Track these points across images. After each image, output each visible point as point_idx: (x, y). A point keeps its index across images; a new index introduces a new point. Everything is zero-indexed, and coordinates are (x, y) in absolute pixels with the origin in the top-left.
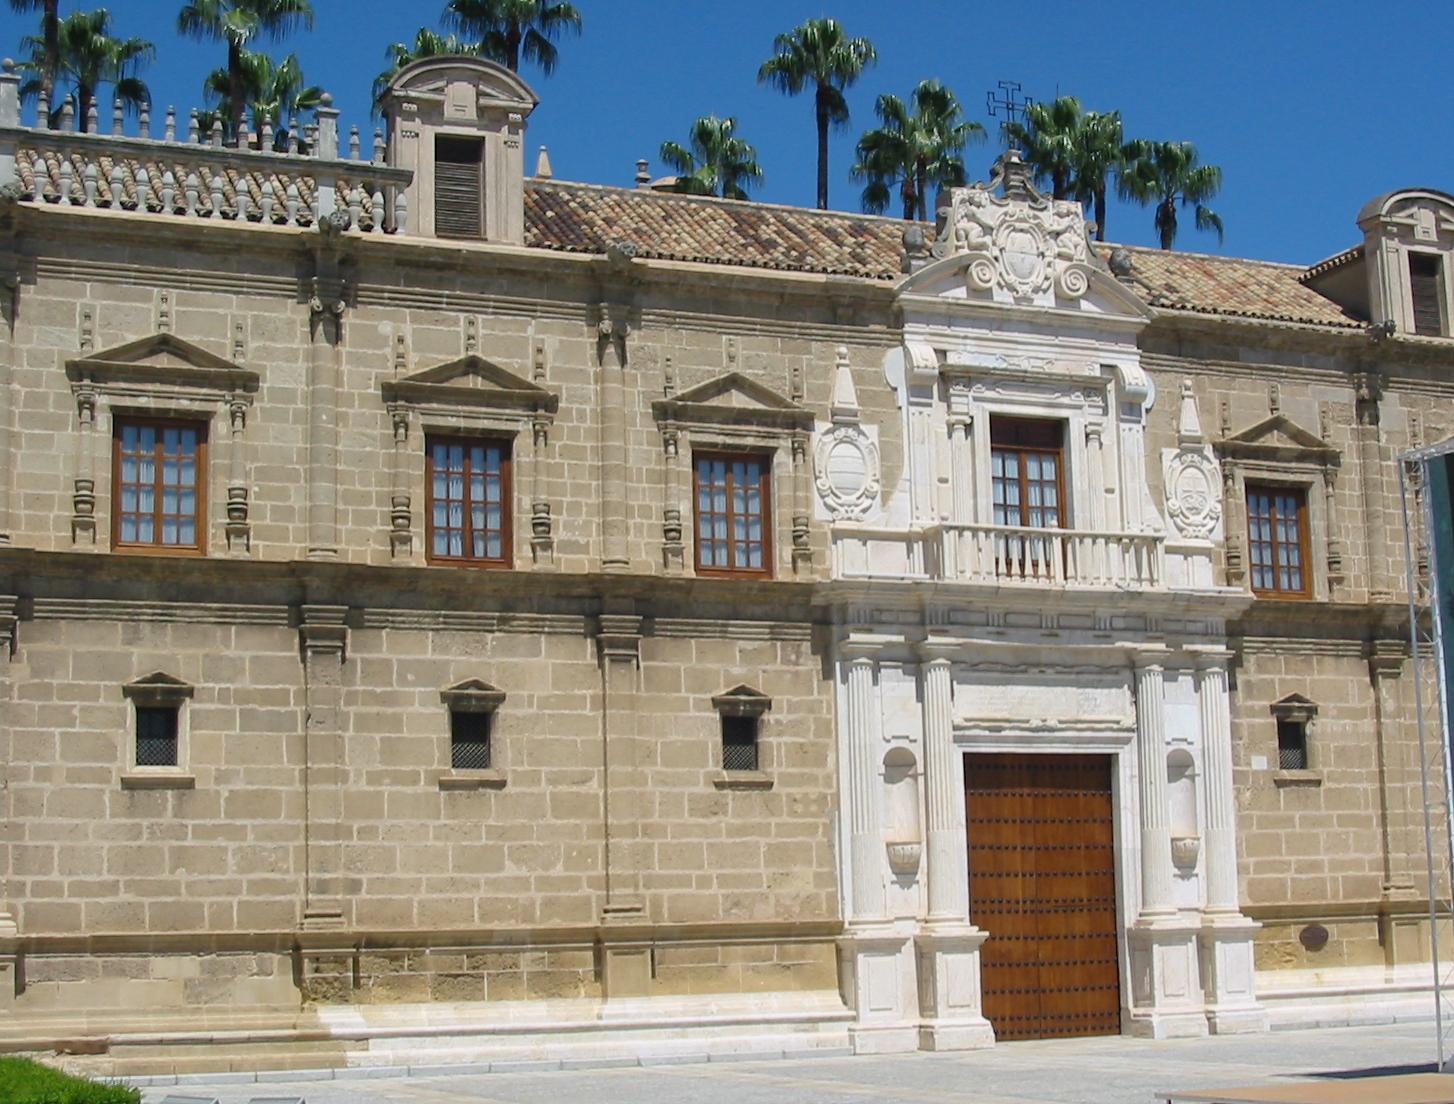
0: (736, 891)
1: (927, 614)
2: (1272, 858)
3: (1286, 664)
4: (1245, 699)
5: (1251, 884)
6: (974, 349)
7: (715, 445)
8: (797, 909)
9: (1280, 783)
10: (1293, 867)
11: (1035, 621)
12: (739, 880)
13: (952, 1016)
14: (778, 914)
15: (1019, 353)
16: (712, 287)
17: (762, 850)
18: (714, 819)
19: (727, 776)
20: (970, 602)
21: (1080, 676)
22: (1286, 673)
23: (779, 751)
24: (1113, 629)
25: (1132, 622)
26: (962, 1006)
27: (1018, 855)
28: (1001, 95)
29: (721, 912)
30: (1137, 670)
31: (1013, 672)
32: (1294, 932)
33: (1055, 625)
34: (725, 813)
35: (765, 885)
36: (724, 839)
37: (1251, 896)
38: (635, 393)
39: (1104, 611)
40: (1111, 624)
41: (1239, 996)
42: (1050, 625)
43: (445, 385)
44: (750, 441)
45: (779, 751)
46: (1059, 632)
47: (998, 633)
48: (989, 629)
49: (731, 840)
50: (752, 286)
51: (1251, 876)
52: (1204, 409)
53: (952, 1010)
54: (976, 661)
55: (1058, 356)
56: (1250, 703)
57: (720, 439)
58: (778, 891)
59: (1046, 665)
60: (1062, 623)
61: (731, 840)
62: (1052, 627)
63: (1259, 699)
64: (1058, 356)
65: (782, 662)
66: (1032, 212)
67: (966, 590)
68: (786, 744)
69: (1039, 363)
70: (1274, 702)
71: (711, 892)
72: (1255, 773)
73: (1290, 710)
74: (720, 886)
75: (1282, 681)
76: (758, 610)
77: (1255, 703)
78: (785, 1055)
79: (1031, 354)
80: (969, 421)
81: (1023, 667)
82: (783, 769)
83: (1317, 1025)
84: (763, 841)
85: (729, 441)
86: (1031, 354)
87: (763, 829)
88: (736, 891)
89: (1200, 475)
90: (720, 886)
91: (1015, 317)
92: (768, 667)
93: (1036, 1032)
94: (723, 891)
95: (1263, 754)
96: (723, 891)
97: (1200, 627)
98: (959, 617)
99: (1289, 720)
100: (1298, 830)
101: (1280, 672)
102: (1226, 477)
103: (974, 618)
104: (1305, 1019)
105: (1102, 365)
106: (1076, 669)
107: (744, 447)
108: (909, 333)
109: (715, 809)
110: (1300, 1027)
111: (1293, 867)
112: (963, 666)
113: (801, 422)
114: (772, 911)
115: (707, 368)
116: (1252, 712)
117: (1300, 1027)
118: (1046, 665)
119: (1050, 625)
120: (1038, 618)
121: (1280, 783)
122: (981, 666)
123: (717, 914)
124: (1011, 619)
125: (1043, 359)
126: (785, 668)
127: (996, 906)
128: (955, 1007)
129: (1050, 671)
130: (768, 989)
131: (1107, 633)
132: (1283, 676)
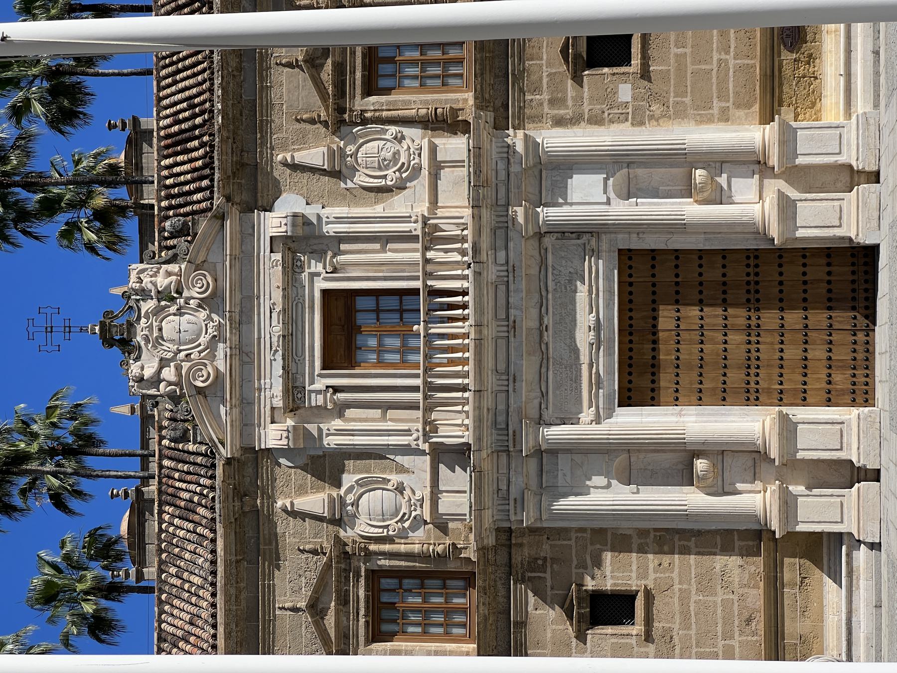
0: (736, 623)
1: (499, 449)
2: (714, 80)
3: (532, 59)
4: (567, 108)
5: (738, 106)
6: (268, 381)
7: (367, 622)
8: (753, 568)
9: (645, 74)
10: (723, 56)
11: (502, 343)
12: (727, 620)
13: (849, 445)
14: (756, 587)
15: (268, 336)
16: (236, 626)
17: (701, 598)
18: (676, 639)
19: (637, 628)
20: (488, 409)
21: (550, 289)
22: (542, 59)
23: (618, 578)
24: (507, 262)
25: (500, 243)
26: (842, 436)
27: (707, 347)
28: (40, 321)
29: (755, 638)
30: (543, 230)
31: (548, 359)
32: (787, 57)
33: (505, 268)
34: (671, 630)
35: (731, 596)
36: (693, 632)
37: (749, 106)
39: (492, 273)
40: (502, 265)
41: (844, 141)
42: (505, 329)
43: (333, 635)
44: (362, 593)
45: (618, 578)
46: (512, 318)
47: (514, 382)
48: (511, 390)
49: (694, 626)
50: (233, 591)
51: (730, 104)
52: (303, 141)
53: (845, 445)
54: (539, 394)
55: (267, 296)
56: (570, 103)
57: (362, 621)
58: (736, 585)
59: (541, 325)
60: (504, 262)
61: (694, 626)
62: (508, 326)
63: (565, 91)
64: (267, 296)
65: (545, 572)
66: (143, 320)
67: (479, 421)
68: (612, 572)
69: (275, 315)
70: (570, 77)
71: (737, 645)
72: (634, 98)
73: (577, 56)
74: (732, 637)
75: (549, 65)
76: (502, 592)
77: (569, 95)
78: (878, 606)
80: (331, 390)
81: (543, 347)
82: (634, 575)
83: (876, 53)
84: (694, 598)
85: (362, 612)
87: (684, 597)
88: (736, 623)
89: (366, 496)
90: (732, 637)
91: (235, 339)
92: (549, 584)
93: (868, 335)
94: (737, 634)
95: (618, 86)
96: (737, 634)
97: (501, 166)
98: (501, 418)
99: (585, 56)
100: (688, 50)
101: (541, 66)
102: (364, 122)
103: (502, 407)
104: (870, 63)
105: (272, 251)
106: (544, 293)
107: (367, 597)
108: (260, 445)
109: (668, 638)
110: (877, 74)
111: (723, 56)
112: (543, 406)
114: (754, 592)
115: (303, 629)
116: (578, 100)
117: (877, 74)
118: (541, 325)
119: (505, 329)
120: (499, 341)
121: (645, 74)
122: (544, 390)
123: (757, 641)
124: (502, 367)
125: (271, 312)
126: (549, 570)
127: (752, 287)
128: (842, 443)
129: (546, 320)
130: (821, 606)
131: (511, 269)
132: (544, 62)
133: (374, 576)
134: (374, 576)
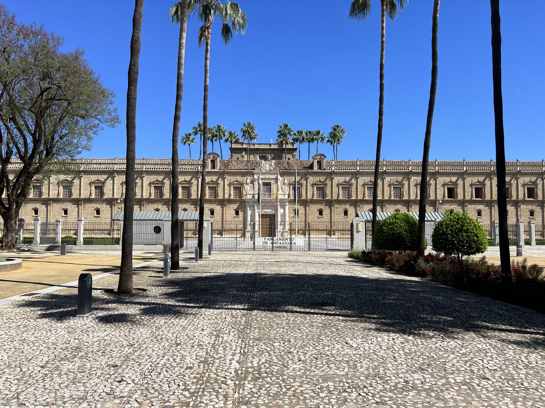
38: (227, 183)
79: (267, 176)
86: (267, 176)
113: (243, 184)
133: (324, 188)
134: (161, 187)
